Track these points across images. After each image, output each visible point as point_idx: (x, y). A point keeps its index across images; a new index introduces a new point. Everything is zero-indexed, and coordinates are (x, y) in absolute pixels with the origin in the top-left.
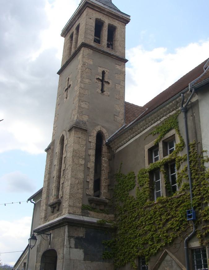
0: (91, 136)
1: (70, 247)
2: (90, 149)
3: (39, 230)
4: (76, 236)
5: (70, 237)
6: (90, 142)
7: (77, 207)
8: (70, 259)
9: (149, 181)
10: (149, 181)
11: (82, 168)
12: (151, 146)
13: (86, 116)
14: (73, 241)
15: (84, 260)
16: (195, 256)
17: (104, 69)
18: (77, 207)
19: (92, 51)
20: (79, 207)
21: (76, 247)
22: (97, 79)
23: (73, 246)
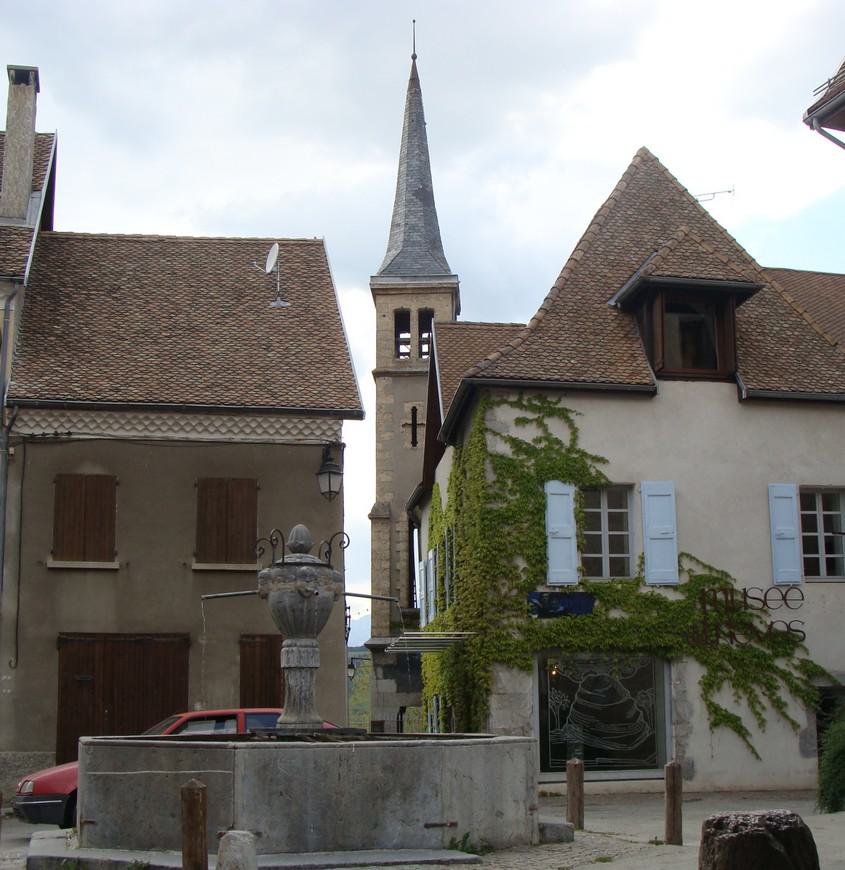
0: (398, 522)
1: (377, 679)
2: (398, 542)
3: (156, 639)
4: (383, 664)
5: (376, 666)
6: (398, 532)
7: (382, 627)
8: (378, 693)
9: (651, 646)
10: (651, 646)
11: (387, 573)
12: (238, 690)
13: (390, 494)
14: (380, 671)
15: (398, 691)
16: (360, 614)
17: (414, 404)
18: (382, 627)
19: (390, 379)
20: (386, 627)
21: (385, 678)
22: (404, 426)
23: (380, 676)
